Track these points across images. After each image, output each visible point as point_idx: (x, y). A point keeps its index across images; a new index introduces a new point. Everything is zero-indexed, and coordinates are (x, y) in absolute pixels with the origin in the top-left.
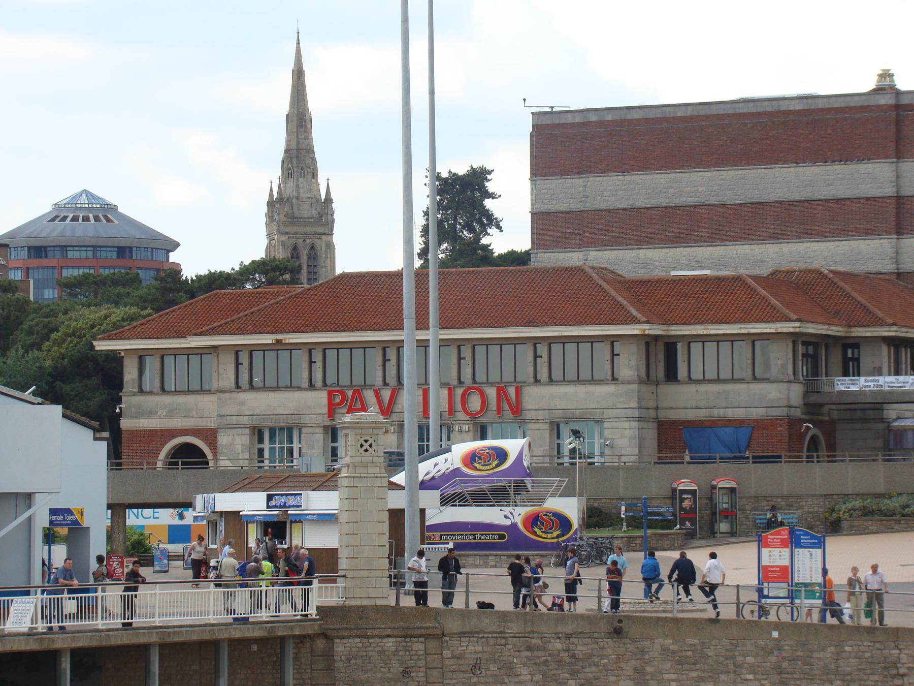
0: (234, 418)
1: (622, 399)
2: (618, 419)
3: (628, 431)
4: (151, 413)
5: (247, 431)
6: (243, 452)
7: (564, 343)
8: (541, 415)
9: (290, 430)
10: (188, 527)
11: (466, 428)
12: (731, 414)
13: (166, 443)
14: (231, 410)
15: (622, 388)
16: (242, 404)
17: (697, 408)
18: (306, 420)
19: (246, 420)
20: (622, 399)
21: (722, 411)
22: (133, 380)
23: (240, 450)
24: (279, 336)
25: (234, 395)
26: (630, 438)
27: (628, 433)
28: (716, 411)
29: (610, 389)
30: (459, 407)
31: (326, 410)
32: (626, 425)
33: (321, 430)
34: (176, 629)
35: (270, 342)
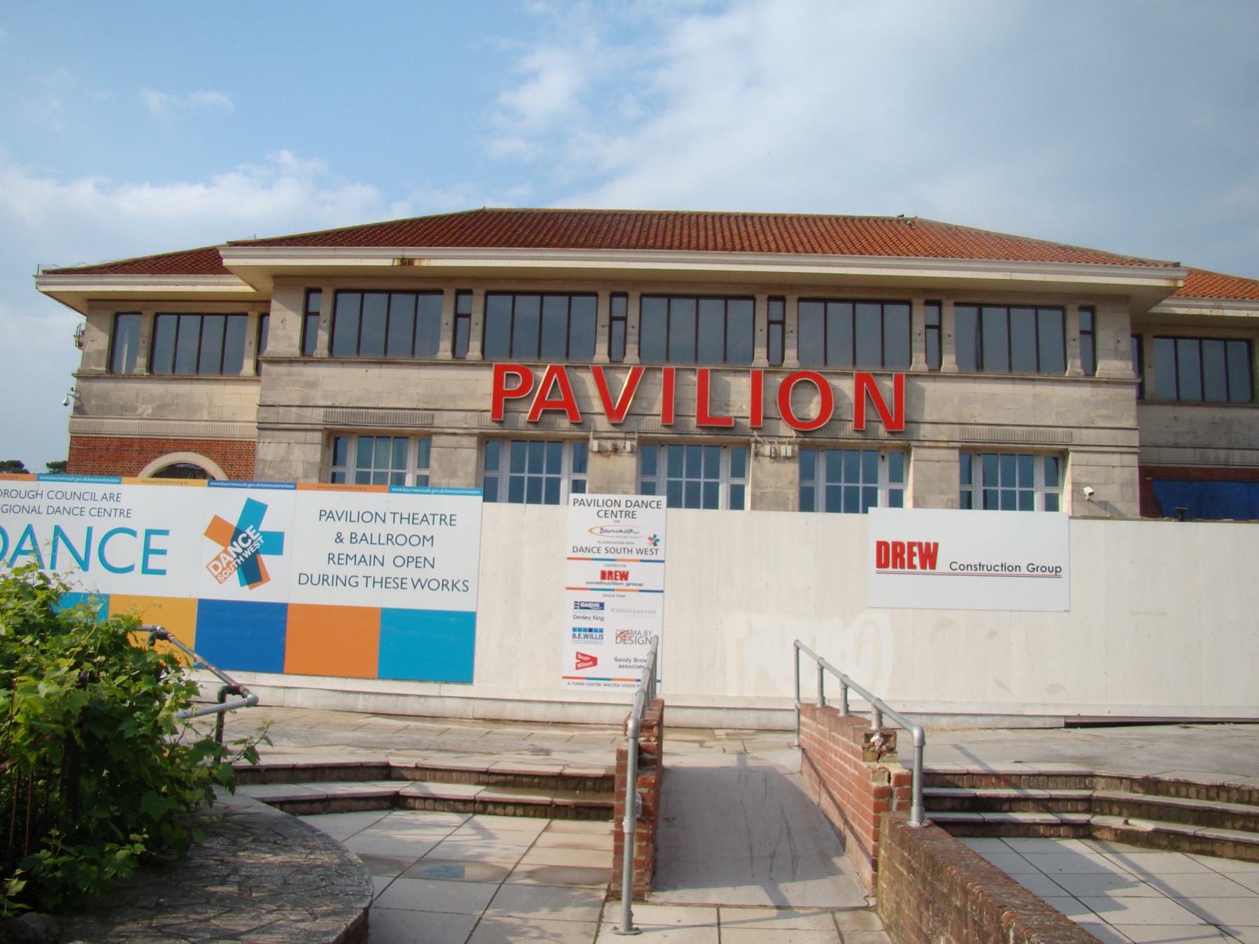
0: (294, 410)
1: (1105, 412)
2: (1100, 449)
3: (1118, 470)
4: (125, 410)
5: (318, 437)
6: (306, 476)
7: (980, 306)
8: (943, 433)
9: (401, 438)
10: (278, 611)
11: (786, 450)
12: (1237, 458)
13: (147, 461)
14: (290, 394)
15: (1104, 393)
16: (312, 385)
17: (1176, 446)
18: (442, 420)
19: (317, 416)
20: (1105, 412)
21: (1222, 455)
22: (100, 352)
23: (300, 473)
24: (409, 252)
25: (296, 369)
26: (1122, 485)
27: (1118, 474)
28: (1211, 454)
29: (1085, 392)
30: (774, 410)
31: (488, 404)
32: (1115, 459)
33: (473, 441)
34: (355, 411)
35: (388, 263)
